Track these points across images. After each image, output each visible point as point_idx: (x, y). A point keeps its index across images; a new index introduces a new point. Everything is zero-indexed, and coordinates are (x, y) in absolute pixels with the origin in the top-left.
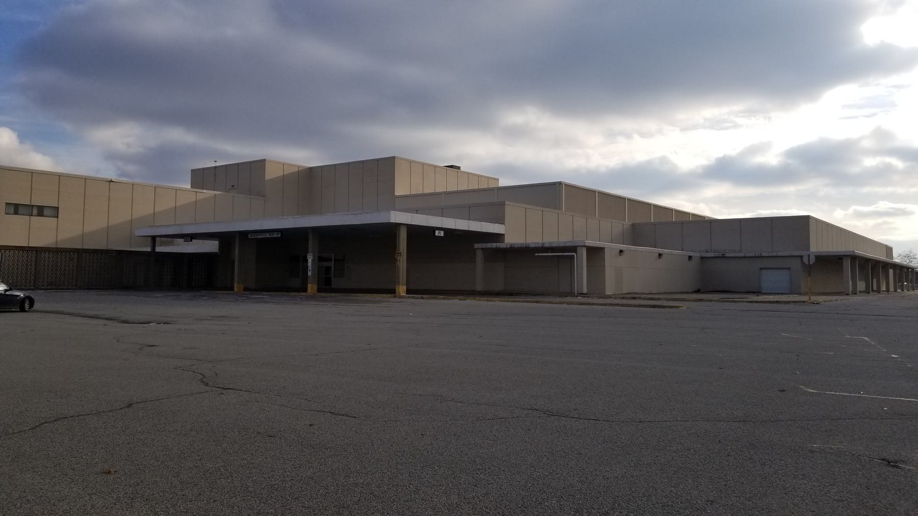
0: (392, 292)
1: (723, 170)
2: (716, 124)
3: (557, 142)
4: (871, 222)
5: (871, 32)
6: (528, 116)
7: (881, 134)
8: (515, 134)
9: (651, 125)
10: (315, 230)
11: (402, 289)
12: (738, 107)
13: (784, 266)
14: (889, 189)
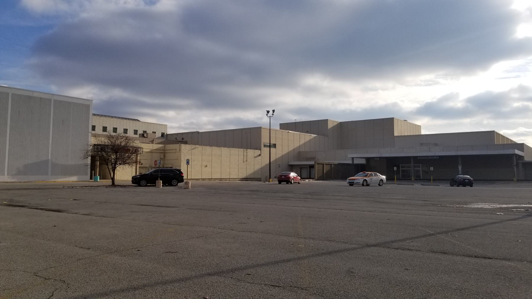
0: (513, 180)
1: (429, 110)
2: (428, 84)
3: (334, 95)
4: (522, 138)
5: (522, 31)
6: (313, 80)
7: (522, 89)
8: (311, 90)
9: (390, 84)
10: (461, 156)
11: (413, 179)
12: (441, 73)
13: (479, 162)
14: (526, 120)
